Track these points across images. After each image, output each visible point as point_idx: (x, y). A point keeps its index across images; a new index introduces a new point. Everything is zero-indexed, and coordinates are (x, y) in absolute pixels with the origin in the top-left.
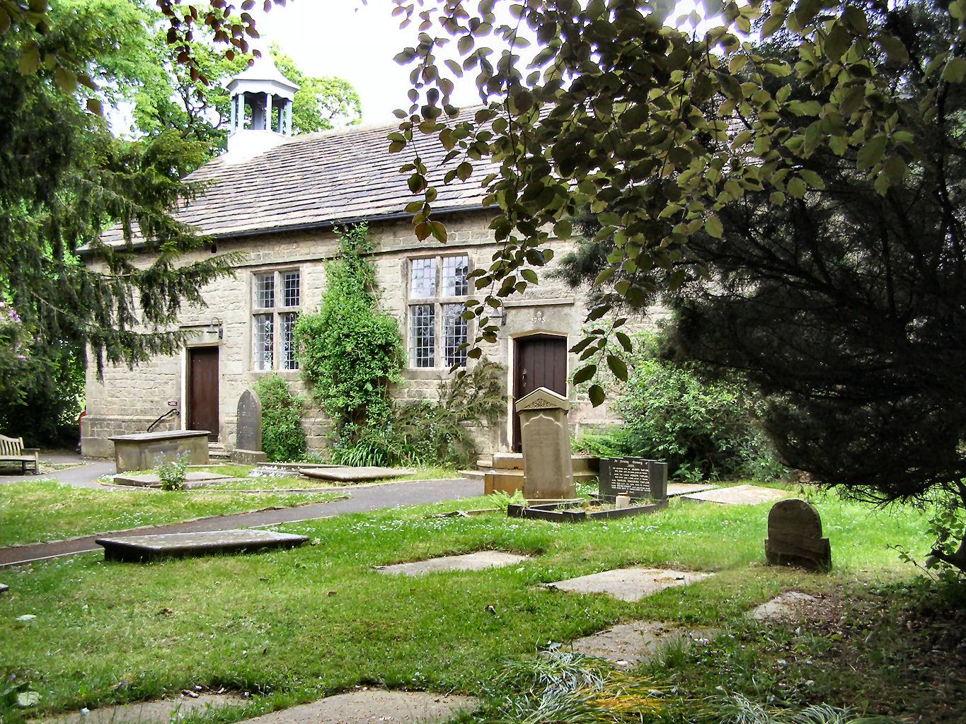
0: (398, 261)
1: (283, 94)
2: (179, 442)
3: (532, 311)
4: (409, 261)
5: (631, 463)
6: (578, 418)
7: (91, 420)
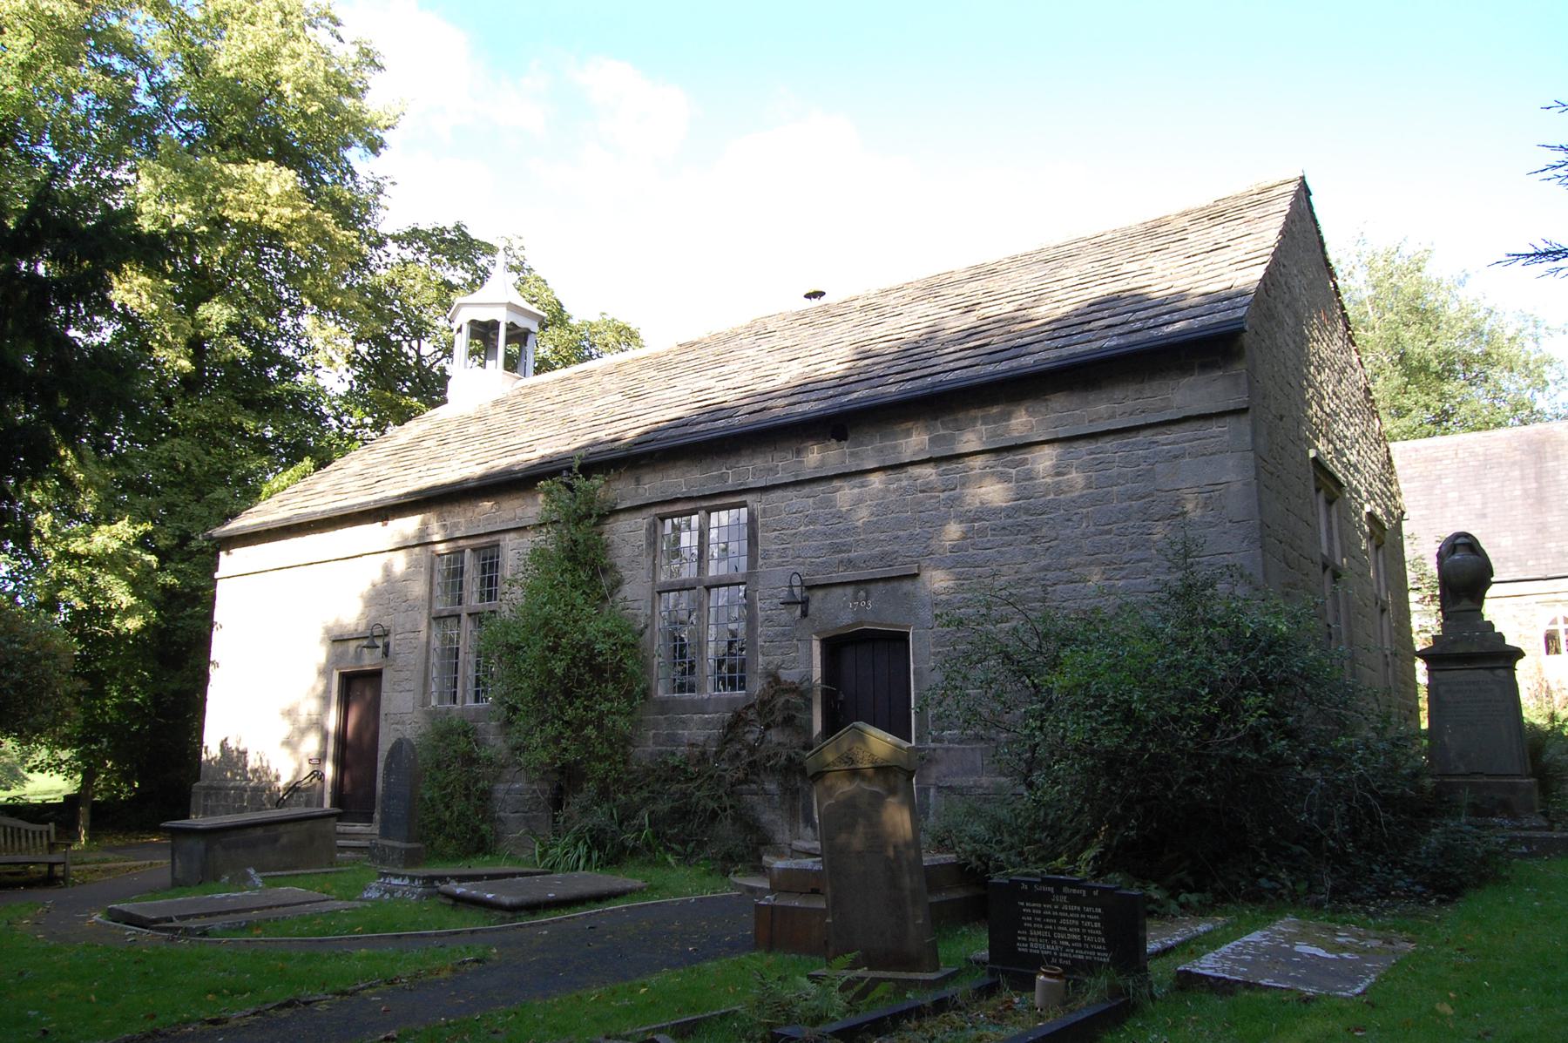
0: (641, 521)
1: (523, 323)
2: (281, 828)
3: (850, 590)
4: (659, 522)
5: (1059, 892)
6: (934, 775)
7: (205, 788)
